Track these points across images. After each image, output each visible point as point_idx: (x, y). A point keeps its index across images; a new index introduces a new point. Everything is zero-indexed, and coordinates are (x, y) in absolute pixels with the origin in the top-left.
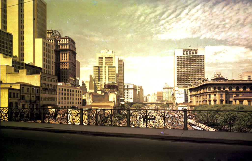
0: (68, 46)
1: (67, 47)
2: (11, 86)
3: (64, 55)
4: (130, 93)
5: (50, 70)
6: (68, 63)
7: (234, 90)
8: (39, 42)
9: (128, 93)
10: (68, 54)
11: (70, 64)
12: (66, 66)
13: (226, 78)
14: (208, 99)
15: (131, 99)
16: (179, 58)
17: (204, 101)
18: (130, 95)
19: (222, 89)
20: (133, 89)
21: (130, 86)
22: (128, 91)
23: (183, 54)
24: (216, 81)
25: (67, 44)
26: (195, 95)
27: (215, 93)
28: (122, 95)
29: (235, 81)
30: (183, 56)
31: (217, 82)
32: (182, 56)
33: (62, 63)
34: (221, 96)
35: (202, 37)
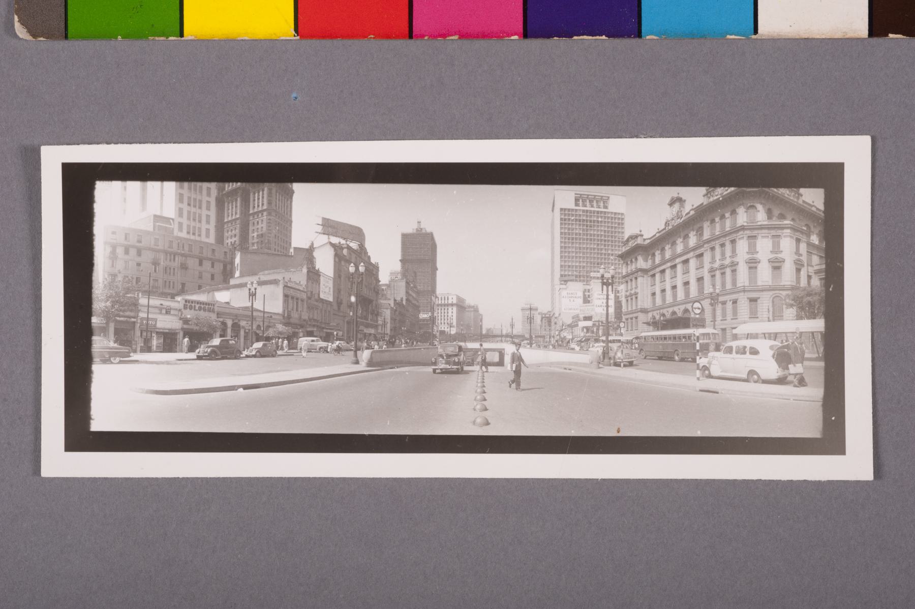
3: (259, 195)
4: (450, 314)
5: (198, 225)
6: (265, 214)
9: (446, 314)
11: (269, 214)
17: (629, 298)
20: (457, 305)
21: (449, 298)
22: (446, 309)
23: (577, 205)
28: (194, 234)
32: (573, 210)
33: (253, 217)
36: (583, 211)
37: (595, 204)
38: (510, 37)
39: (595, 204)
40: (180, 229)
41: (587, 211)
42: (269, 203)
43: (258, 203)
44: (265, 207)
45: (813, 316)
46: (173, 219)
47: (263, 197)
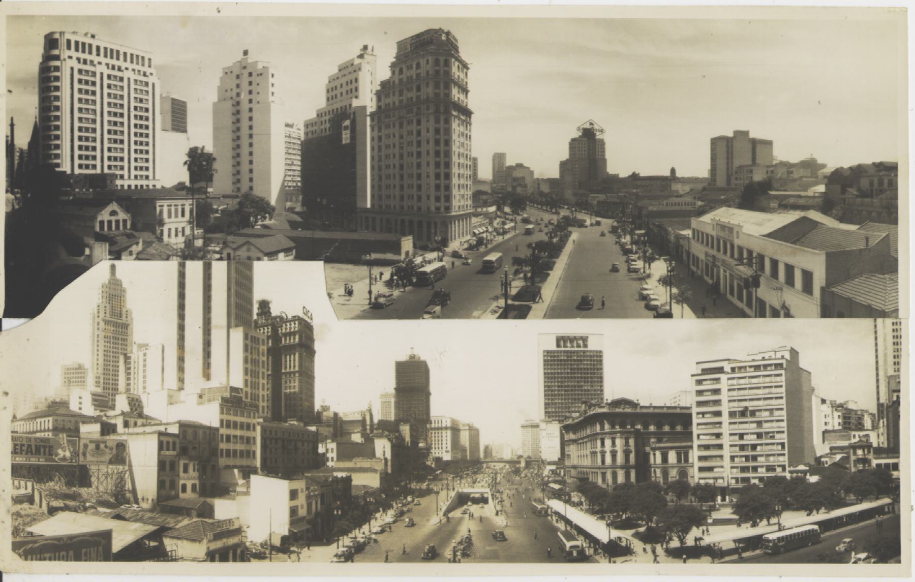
0: (297, 337)
1: (294, 339)
2: (166, 429)
4: (444, 439)
6: (297, 375)
7: (652, 428)
8: (238, 335)
9: (440, 438)
10: (297, 355)
11: (300, 375)
12: (292, 381)
13: (636, 401)
14: (599, 449)
15: (447, 452)
16: (548, 353)
18: (444, 442)
19: (629, 427)
23: (558, 345)
24: (616, 407)
25: (294, 333)
26: (574, 441)
27: (614, 436)
29: (655, 407)
30: (558, 352)
31: (617, 410)
32: (554, 352)
34: (627, 444)
35: (374, 413)
36: (565, 352)
37: (569, 344)
38: (797, 466)
39: (569, 344)
40: (247, 398)
41: (567, 352)
42: (301, 365)
43: (290, 364)
44: (297, 369)
45: (234, 472)
46: (241, 389)
47: (294, 360)
